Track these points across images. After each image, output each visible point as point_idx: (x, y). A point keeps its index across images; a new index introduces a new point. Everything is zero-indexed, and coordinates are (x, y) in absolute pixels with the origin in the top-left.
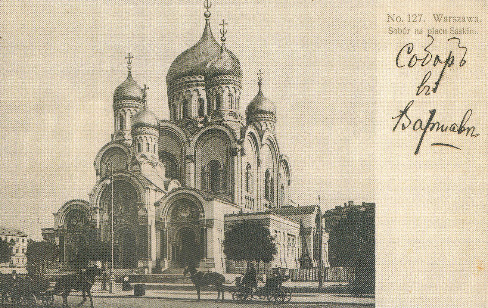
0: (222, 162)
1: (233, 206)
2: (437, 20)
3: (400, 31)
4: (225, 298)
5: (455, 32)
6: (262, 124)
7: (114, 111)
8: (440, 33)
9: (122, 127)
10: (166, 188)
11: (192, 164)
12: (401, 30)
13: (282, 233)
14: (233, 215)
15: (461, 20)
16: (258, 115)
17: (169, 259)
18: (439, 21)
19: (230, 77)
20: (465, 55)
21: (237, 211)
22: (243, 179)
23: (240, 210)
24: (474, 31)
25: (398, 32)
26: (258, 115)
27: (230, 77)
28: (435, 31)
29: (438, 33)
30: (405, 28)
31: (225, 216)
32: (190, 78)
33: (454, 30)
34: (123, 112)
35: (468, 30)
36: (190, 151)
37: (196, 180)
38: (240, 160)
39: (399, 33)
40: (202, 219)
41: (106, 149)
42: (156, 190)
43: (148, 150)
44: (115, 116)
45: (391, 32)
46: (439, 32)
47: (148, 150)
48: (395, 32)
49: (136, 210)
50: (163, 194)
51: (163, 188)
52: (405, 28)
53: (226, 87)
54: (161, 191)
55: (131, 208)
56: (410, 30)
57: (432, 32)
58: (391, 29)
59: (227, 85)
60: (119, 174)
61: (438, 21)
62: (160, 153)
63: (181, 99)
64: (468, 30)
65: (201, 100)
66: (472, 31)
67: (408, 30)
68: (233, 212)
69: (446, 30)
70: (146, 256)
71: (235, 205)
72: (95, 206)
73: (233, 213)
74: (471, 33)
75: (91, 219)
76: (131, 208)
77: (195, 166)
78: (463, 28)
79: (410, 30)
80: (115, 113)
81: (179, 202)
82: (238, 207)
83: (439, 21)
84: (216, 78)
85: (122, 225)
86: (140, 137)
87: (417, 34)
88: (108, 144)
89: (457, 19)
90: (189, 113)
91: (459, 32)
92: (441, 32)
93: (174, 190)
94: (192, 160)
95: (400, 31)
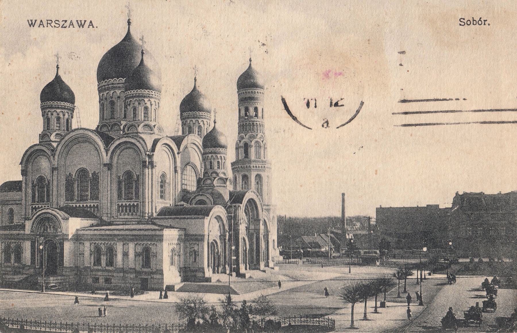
0: (136, 172)
3: (475, 22)
4: (159, 292)
15: (67, 24)
18: (83, 27)
19: (149, 92)
20: (416, 125)
25: (472, 23)
27: (149, 92)
30: (481, 18)
33: (465, 21)
37: (238, 153)
38: (150, 173)
39: (473, 24)
40: (60, 233)
53: (67, 112)
56: (486, 20)
58: (462, 20)
59: (62, 110)
61: (81, 27)
79: (486, 20)
83: (83, 27)
84: (135, 92)
95: (475, 22)
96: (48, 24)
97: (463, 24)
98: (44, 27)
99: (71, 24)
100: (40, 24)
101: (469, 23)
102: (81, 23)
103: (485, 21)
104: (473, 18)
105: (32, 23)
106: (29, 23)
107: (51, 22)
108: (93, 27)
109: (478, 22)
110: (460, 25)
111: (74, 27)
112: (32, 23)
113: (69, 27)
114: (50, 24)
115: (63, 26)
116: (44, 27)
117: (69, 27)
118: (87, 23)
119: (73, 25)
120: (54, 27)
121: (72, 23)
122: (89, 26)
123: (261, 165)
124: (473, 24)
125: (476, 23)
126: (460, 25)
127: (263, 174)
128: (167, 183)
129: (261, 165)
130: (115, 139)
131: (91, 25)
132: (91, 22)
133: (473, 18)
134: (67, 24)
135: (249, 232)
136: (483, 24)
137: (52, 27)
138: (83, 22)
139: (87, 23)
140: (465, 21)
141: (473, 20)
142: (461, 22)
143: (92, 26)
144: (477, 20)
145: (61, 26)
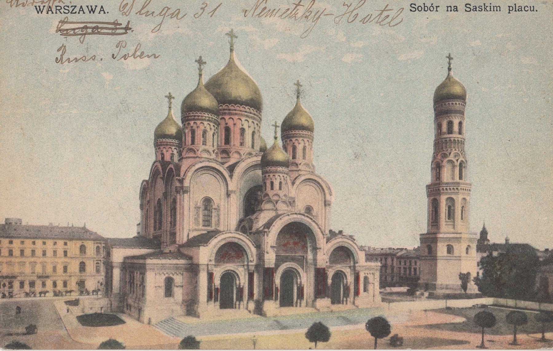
2: (38, 11)
3: (426, 9)
5: (472, 9)
6: (300, 142)
15: (77, 10)
16: (289, 132)
17: (276, 299)
18: (42, 13)
22: (460, 212)
24: (498, 8)
26: (289, 132)
28: (517, 8)
29: (521, 10)
30: (432, 4)
33: (416, 7)
34: (296, 142)
39: (424, 10)
46: (523, 9)
48: (420, 9)
52: (432, 4)
56: (439, 6)
57: (514, 8)
61: (40, 12)
64: (490, 6)
66: (495, 8)
67: (437, 7)
69: (533, 7)
78: (484, 4)
79: (439, 6)
82: (224, 233)
83: (42, 13)
89: (71, 9)
91: (478, 9)
96: (56, 10)
97: (414, 9)
98: (53, 13)
99: (81, 9)
100: (101, 10)
101: (526, 9)
102: (40, 8)
103: (437, 7)
104: (424, 4)
105: (92, 9)
106: (89, 9)
107: (60, 8)
108: (105, 13)
109: (430, 8)
110: (466, 11)
111: (84, 13)
112: (40, 9)
113: (79, 13)
114: (59, 10)
115: (73, 12)
116: (53, 13)
117: (79, 13)
118: (98, 9)
119: (83, 10)
120: (63, 13)
121: (82, 9)
122: (100, 12)
123: (452, 187)
124: (424, 10)
125: (428, 9)
126: (466, 11)
127: (458, 199)
128: (215, 209)
129: (452, 187)
130: (253, 154)
131: (50, 11)
132: (102, 7)
133: (424, 4)
134: (77, 10)
135: (397, 283)
136: (435, 10)
137: (61, 13)
138: (42, 8)
139: (98, 9)
140: (416, 7)
141: (425, 7)
142: (480, 8)
143: (103, 12)
144: (429, 5)
145: (70, 11)
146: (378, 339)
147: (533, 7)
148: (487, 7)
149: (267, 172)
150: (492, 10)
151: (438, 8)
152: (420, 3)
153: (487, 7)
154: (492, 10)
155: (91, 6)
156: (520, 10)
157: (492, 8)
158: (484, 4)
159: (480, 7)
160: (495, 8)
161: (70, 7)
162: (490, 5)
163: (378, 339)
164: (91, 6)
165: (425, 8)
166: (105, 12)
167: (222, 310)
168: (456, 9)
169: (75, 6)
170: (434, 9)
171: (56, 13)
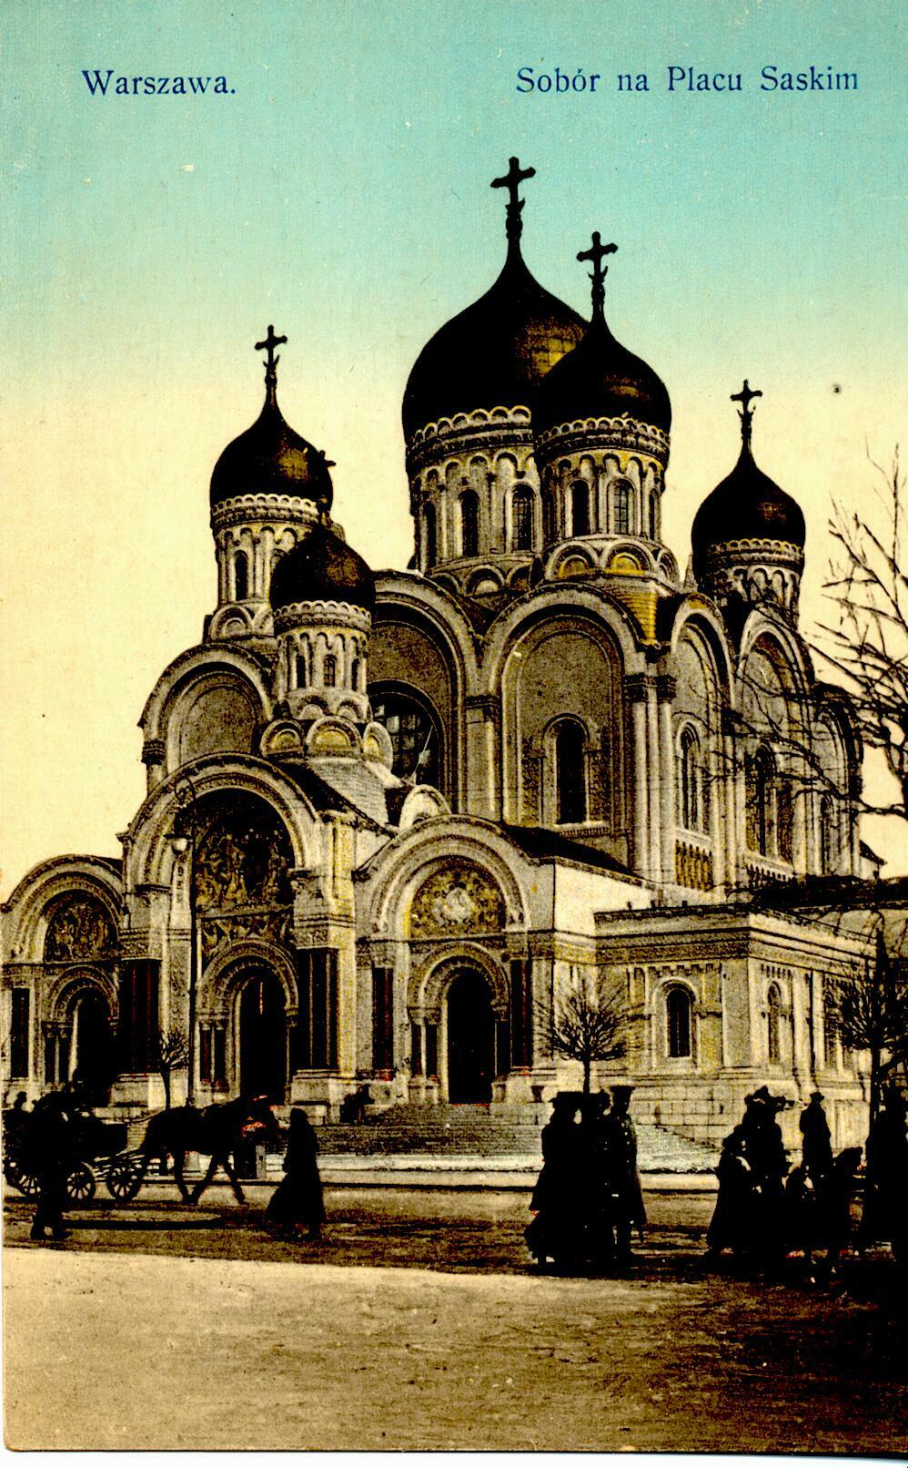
1: (627, 881)
3: (562, 82)
5: (780, 82)
7: (215, 534)
8: (716, 87)
9: (242, 592)
10: (394, 817)
11: (490, 725)
12: (565, 77)
13: (799, 975)
14: (627, 914)
21: (642, 900)
23: (655, 895)
24: (851, 80)
30: (580, 71)
31: (600, 917)
32: (505, 416)
33: (778, 75)
35: (829, 76)
36: (480, 680)
41: (187, 668)
42: (355, 825)
43: (330, 681)
44: (220, 550)
45: (525, 85)
46: (711, 85)
47: (330, 681)
48: (545, 83)
49: (287, 896)
50: (384, 839)
51: (382, 818)
54: (375, 828)
55: (271, 887)
56: (598, 77)
60: (231, 768)
61: (98, 89)
62: (372, 689)
63: (455, 488)
64: (829, 76)
65: (523, 492)
66: (842, 80)
67: (593, 78)
68: (629, 905)
69: (739, 77)
70: (327, 1061)
71: (633, 879)
72: (140, 881)
73: (627, 909)
74: (847, 87)
75: (129, 928)
76: (271, 887)
77: (499, 731)
78: (812, 69)
80: (217, 542)
81: (435, 867)
85: (236, 949)
86: (304, 636)
87: (625, 91)
88: (193, 652)
90: (438, 524)
91: (795, 83)
92: (720, 82)
93: (422, 821)
94: (487, 713)
103: (593, 78)
146: (581, 1089)
147: (739, 77)
148: (820, 76)
149: (243, 517)
150: (834, 85)
151: (596, 80)
152: (544, 68)
153: (820, 76)
154: (834, 85)
155: (97, 73)
156: (705, 84)
157: (834, 79)
158: (812, 69)
159: (802, 78)
160: (842, 80)
161: (157, 80)
162: (829, 72)
163: (581, 1089)
164: (97, 73)
165: (563, 82)
166: (227, 89)
167: (592, 916)
168: (643, 84)
169: (167, 80)
170: (714, 83)
171: (813, 88)
